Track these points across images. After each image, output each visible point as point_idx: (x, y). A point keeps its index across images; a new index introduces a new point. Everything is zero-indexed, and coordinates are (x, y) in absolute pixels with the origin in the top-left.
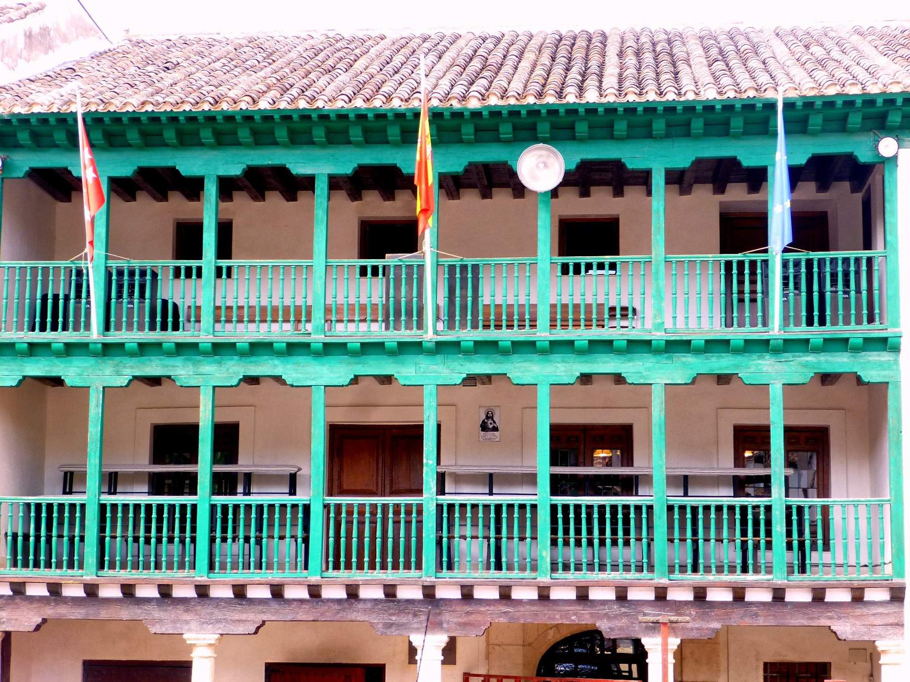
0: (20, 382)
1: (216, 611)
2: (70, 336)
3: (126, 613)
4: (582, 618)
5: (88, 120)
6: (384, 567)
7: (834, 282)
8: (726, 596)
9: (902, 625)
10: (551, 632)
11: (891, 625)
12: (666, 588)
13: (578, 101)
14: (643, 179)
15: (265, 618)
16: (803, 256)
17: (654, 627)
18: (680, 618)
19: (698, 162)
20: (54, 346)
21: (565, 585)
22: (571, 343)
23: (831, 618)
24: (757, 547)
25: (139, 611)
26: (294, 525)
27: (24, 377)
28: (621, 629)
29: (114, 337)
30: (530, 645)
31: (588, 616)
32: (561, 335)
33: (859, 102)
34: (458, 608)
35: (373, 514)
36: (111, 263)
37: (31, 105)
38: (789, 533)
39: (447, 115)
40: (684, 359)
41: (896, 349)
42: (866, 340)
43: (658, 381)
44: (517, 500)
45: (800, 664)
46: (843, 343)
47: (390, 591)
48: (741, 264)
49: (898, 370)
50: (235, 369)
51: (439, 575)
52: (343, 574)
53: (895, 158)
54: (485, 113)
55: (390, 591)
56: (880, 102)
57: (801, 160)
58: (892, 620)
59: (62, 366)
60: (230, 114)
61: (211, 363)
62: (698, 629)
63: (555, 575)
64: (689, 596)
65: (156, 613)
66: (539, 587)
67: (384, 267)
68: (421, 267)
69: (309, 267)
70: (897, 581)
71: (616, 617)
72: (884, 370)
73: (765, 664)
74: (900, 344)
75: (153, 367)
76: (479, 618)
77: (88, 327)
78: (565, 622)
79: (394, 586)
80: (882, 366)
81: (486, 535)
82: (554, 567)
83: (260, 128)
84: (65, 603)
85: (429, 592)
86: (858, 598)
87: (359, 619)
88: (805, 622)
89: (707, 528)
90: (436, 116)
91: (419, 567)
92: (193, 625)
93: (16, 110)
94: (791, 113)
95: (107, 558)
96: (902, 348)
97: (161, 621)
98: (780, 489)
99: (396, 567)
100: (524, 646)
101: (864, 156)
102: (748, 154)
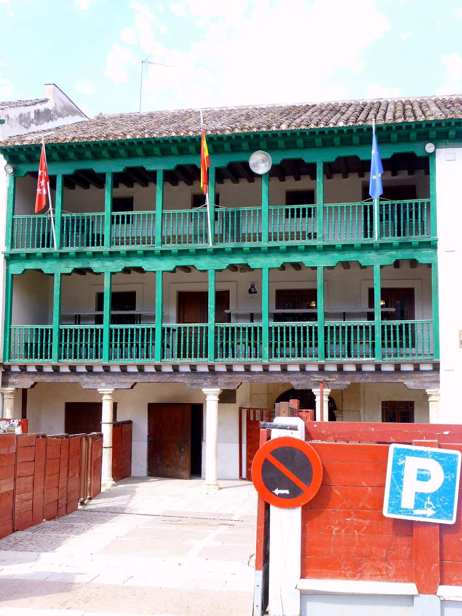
0: (23, 272)
1: (113, 378)
2: (96, 249)
3: (72, 379)
4: (285, 379)
5: (50, 148)
6: (190, 356)
7: (411, 216)
8: (353, 368)
9: (439, 382)
10: (281, 388)
11: (433, 382)
12: (324, 365)
13: (277, 129)
14: (153, 175)
15: (135, 381)
16: (389, 202)
17: (317, 384)
18: (331, 379)
19: (339, 159)
20: (37, 254)
21: (275, 364)
22: (278, 248)
23: (404, 379)
24: (305, 345)
25: (78, 378)
26: (244, 337)
27: (25, 270)
28: (303, 385)
29: (65, 250)
30: (271, 394)
31: (287, 379)
32: (273, 244)
33: (414, 126)
34: (226, 376)
35: (407, 329)
36: (63, 215)
37: (23, 141)
38: (383, 339)
39: (215, 139)
40: (333, 255)
41: (435, 247)
42: (420, 243)
43: (320, 265)
44: (145, 326)
45: (399, 402)
46: (409, 245)
47: (193, 368)
48: (399, 205)
49: (437, 258)
50: (121, 264)
51: (216, 360)
52: (279, 360)
53: (434, 153)
54: (233, 137)
55: (193, 368)
56: (424, 125)
57: (388, 155)
58: (433, 380)
59: (42, 264)
60: (275, 133)
61: (109, 261)
62: (340, 384)
63: (271, 360)
64: (335, 369)
65: (86, 379)
66: (433, 364)
67: (314, 208)
68: (371, 207)
69: (154, 215)
70: (435, 360)
71: (300, 379)
72: (430, 257)
73: (383, 402)
74: (436, 244)
75: (185, 261)
76: (235, 380)
77: (53, 246)
78: (276, 382)
79: (195, 366)
80: (428, 255)
81: (244, 341)
82: (383, 356)
83: (130, 148)
84: (45, 375)
85: (211, 368)
86: (417, 369)
87: (179, 381)
88: (391, 381)
89: (332, 337)
90: (210, 140)
91: (206, 356)
92: (103, 384)
93: (17, 144)
94: (380, 133)
95: (123, 354)
96: (438, 246)
97: (87, 383)
98: (379, 316)
99: (196, 356)
100: (268, 394)
101: (419, 153)
102: (360, 153)
